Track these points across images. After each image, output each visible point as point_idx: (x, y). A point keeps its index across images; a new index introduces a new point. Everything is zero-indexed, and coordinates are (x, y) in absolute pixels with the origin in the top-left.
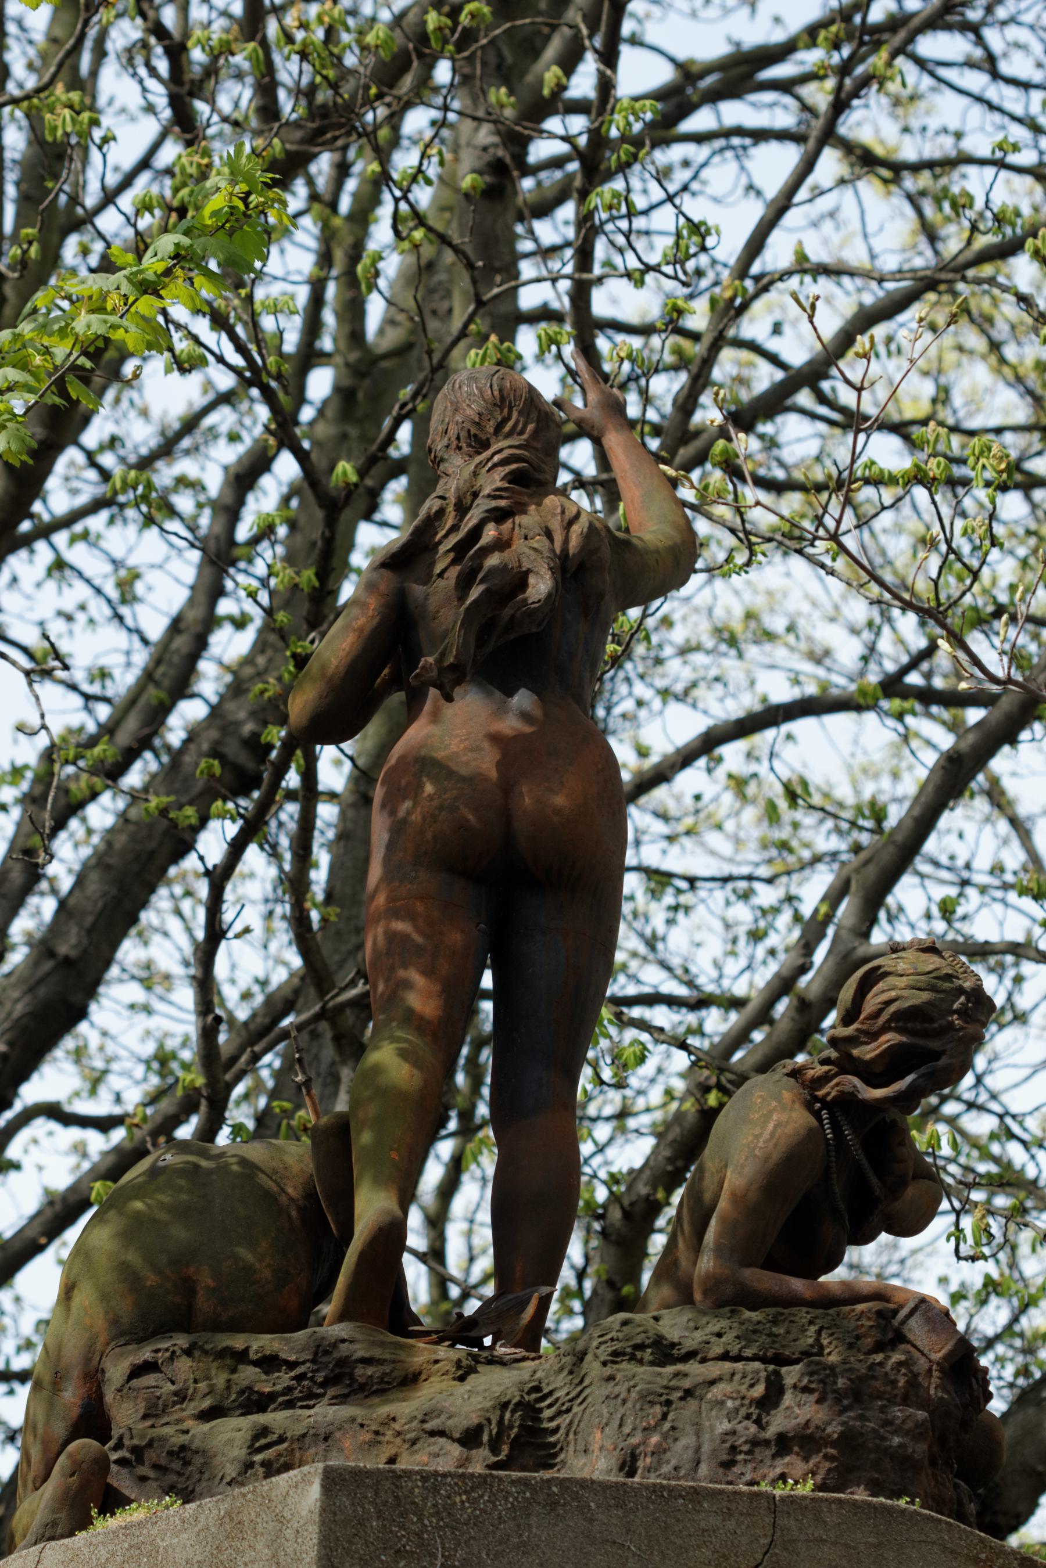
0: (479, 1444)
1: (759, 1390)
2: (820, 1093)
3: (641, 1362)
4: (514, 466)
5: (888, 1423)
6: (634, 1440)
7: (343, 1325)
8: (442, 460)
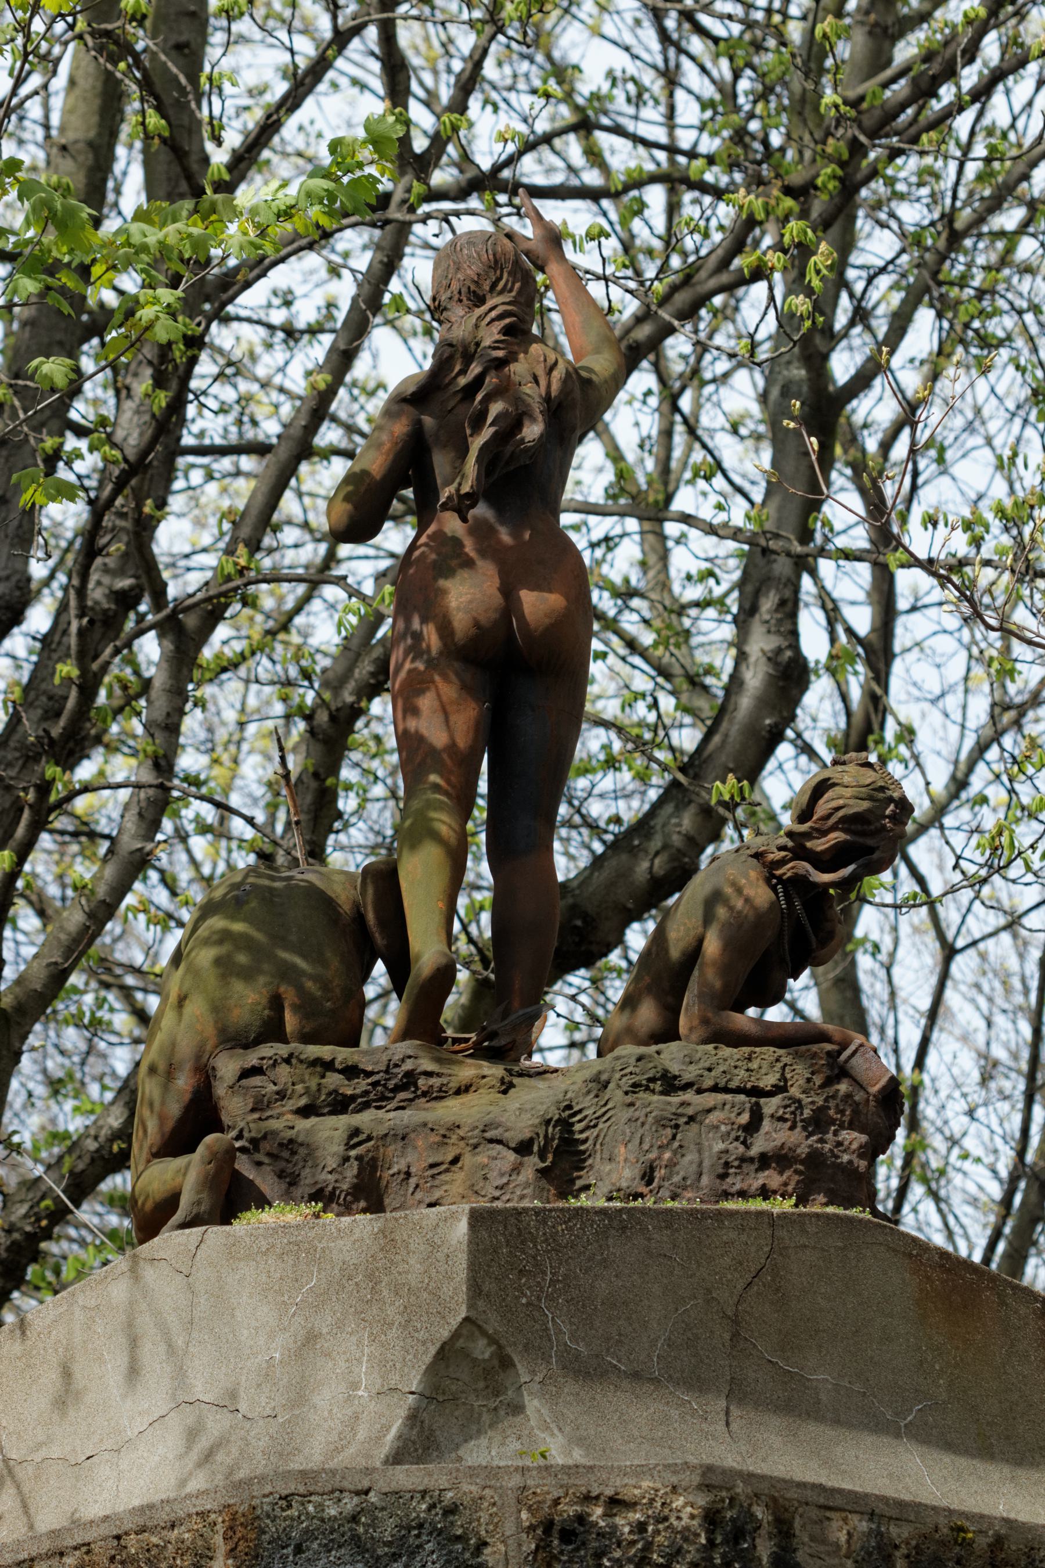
0: (529, 1152)
1: (745, 1118)
2: (778, 872)
3: (653, 1091)
4: (507, 321)
5: (839, 1144)
6: (652, 1156)
7: (408, 1042)
8: (446, 309)
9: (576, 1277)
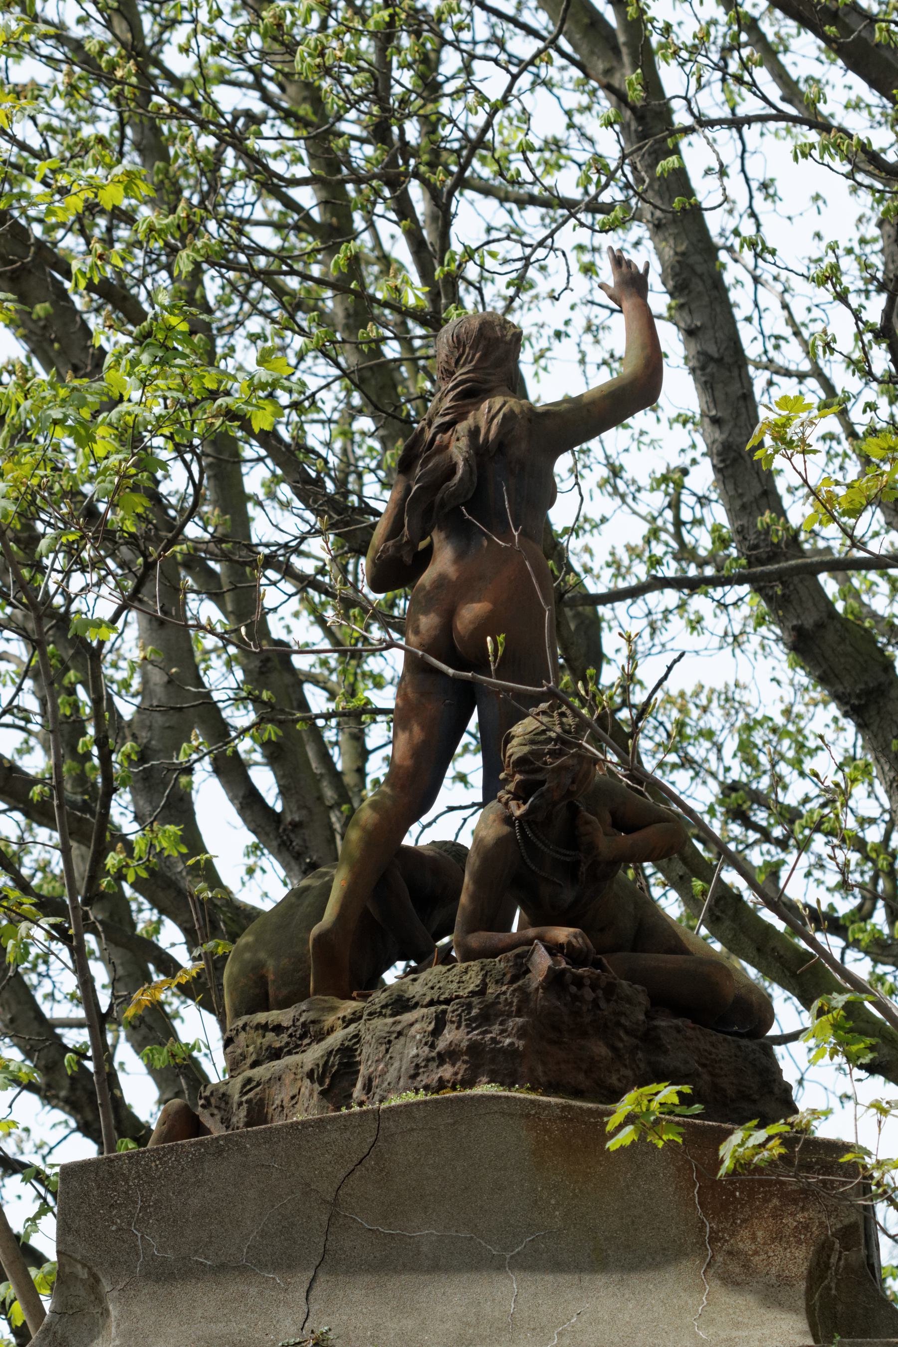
9: (169, 1199)
